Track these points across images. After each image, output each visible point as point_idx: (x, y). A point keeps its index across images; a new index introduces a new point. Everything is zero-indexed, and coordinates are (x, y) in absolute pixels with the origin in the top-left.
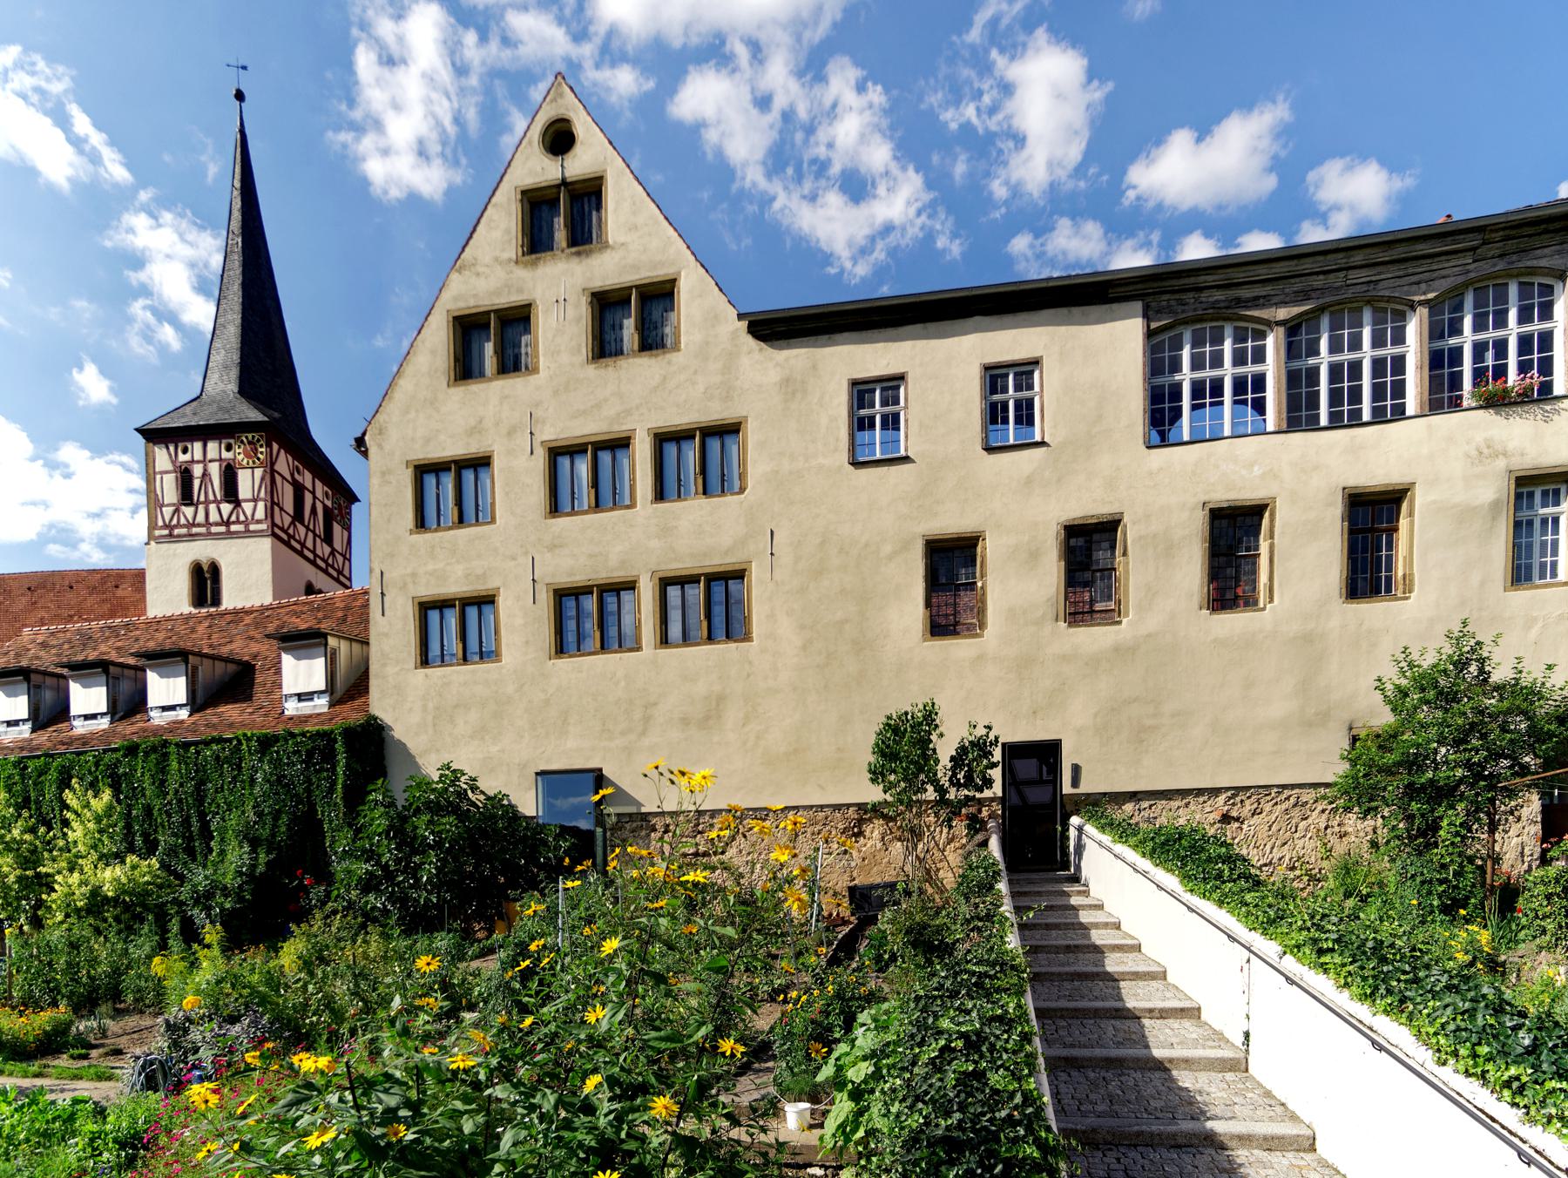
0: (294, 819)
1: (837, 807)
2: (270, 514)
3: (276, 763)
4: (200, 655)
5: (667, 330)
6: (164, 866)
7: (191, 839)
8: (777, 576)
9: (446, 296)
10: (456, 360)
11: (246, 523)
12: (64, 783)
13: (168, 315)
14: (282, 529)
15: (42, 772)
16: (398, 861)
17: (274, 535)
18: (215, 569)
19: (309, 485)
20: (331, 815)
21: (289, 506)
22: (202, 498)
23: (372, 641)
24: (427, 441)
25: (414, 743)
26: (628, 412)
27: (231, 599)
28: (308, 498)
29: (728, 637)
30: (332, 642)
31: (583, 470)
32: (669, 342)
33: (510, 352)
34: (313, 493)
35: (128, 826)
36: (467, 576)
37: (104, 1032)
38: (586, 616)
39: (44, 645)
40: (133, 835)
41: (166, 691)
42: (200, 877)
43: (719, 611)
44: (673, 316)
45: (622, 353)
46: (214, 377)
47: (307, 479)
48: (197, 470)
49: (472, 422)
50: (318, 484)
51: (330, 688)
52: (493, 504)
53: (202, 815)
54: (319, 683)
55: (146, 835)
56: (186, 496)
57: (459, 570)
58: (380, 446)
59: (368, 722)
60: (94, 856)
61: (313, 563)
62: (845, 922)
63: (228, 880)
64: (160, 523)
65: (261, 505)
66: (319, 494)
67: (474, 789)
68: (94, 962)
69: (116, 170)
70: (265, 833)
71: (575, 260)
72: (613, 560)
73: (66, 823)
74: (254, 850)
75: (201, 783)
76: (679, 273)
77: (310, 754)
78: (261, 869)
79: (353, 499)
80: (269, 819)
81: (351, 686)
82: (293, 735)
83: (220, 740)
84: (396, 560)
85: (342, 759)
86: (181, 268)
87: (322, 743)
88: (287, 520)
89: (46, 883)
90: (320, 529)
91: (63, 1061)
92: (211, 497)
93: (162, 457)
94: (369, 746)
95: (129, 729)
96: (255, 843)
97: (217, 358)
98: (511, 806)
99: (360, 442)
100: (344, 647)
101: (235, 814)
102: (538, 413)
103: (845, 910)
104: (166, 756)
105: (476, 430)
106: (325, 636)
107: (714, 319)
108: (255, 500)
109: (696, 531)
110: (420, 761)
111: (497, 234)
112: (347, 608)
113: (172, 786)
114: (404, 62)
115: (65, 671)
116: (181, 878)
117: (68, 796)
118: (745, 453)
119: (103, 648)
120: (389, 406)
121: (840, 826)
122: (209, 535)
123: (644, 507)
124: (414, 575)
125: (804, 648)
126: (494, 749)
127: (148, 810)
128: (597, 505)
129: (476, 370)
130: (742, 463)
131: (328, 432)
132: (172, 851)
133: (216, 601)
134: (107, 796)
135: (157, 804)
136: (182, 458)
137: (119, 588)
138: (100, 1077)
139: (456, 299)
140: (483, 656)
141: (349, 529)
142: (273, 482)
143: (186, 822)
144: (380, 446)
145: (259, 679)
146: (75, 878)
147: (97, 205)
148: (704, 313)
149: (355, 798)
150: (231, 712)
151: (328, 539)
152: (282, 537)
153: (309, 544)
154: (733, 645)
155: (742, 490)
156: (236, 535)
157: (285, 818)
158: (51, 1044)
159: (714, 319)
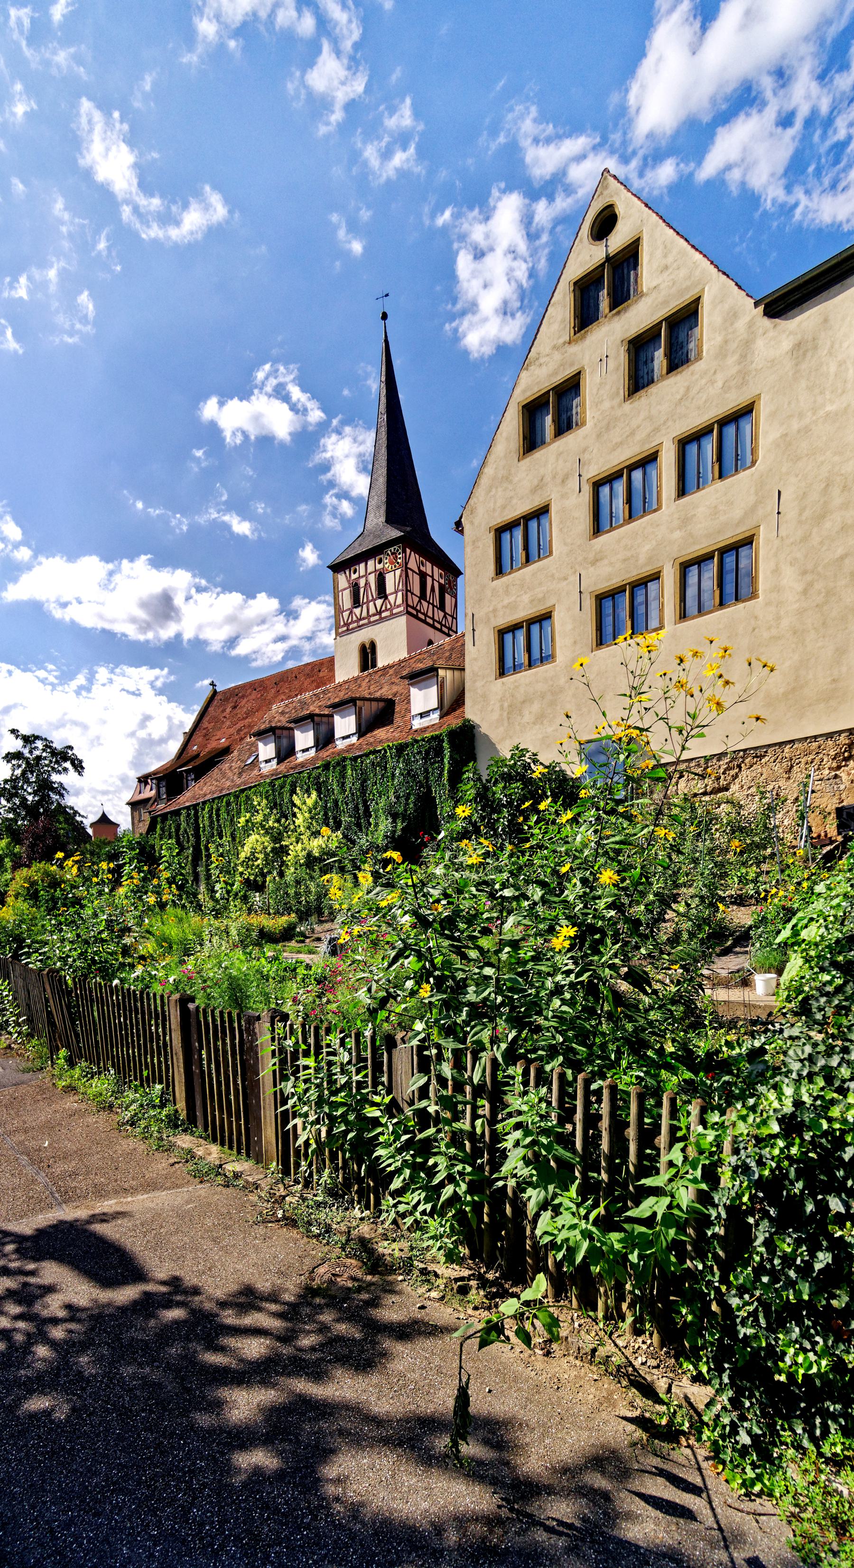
0: (419, 798)
1: (829, 736)
2: (405, 599)
3: (407, 762)
4: (364, 699)
5: (692, 345)
6: (345, 836)
7: (359, 818)
8: (782, 532)
9: (518, 391)
10: (524, 438)
11: (391, 610)
12: (293, 792)
13: (344, 495)
15: (282, 787)
16: (482, 818)
17: (408, 613)
18: (373, 645)
20: (441, 792)
21: (417, 590)
23: (467, 667)
24: (504, 507)
25: (494, 736)
26: (657, 430)
28: (429, 580)
29: (737, 599)
30: (441, 672)
31: (619, 493)
32: (692, 356)
33: (564, 417)
35: (326, 814)
36: (532, 601)
37: (313, 931)
38: (619, 610)
39: (283, 713)
40: (329, 816)
41: (345, 725)
42: (363, 841)
43: (730, 578)
44: (697, 331)
45: (653, 381)
46: (371, 516)
47: (428, 568)
48: (362, 582)
49: (536, 482)
51: (441, 706)
52: (551, 541)
53: (365, 802)
54: (434, 704)
55: (335, 818)
56: (356, 601)
57: (526, 598)
58: (472, 523)
59: (464, 725)
60: (308, 833)
61: (433, 626)
62: (831, 842)
63: (379, 842)
66: (436, 577)
67: (535, 761)
68: (308, 892)
69: (316, 415)
70: (401, 809)
71: (616, 319)
72: (642, 559)
73: (294, 815)
74: (394, 821)
75: (365, 781)
77: (427, 753)
78: (399, 833)
79: (457, 573)
80: (403, 800)
81: (453, 703)
82: (417, 741)
83: (375, 752)
84: (487, 600)
85: (447, 753)
86: (351, 461)
87: (434, 744)
88: (416, 600)
89: (284, 850)
90: (437, 602)
91: (293, 944)
93: (342, 580)
94: (465, 741)
95: (325, 754)
96: (395, 816)
97: (373, 503)
98: (562, 771)
99: (459, 524)
100: (449, 674)
101: (384, 798)
102: (586, 457)
103: (831, 829)
104: (344, 767)
105: (537, 488)
106: (436, 670)
107: (733, 316)
108: (396, 592)
109: (713, 512)
110: (498, 747)
111: (555, 327)
112: (452, 649)
113: (348, 785)
114: (492, 249)
115: (292, 725)
116: (353, 842)
117: (295, 798)
118: (757, 428)
119: (312, 708)
120: (483, 486)
121: (832, 753)
123: (668, 507)
124: (495, 610)
125: (805, 592)
126: (550, 730)
127: (336, 802)
128: (630, 517)
129: (539, 440)
130: (754, 438)
131: (439, 532)
132: (348, 828)
133: (374, 665)
134: (314, 795)
135: (341, 797)
137: (321, 670)
138: (310, 952)
139: (524, 391)
140: (543, 660)
141: (455, 597)
142: (407, 576)
143: (356, 808)
144: (472, 523)
145: (397, 709)
146: (299, 847)
147: (307, 439)
148: (728, 313)
149: (455, 778)
150: (381, 733)
151: (442, 607)
152: (412, 613)
153: (430, 614)
154: (740, 606)
155: (753, 463)
156: (387, 619)
157: (412, 798)
158: (288, 934)
159: (733, 316)
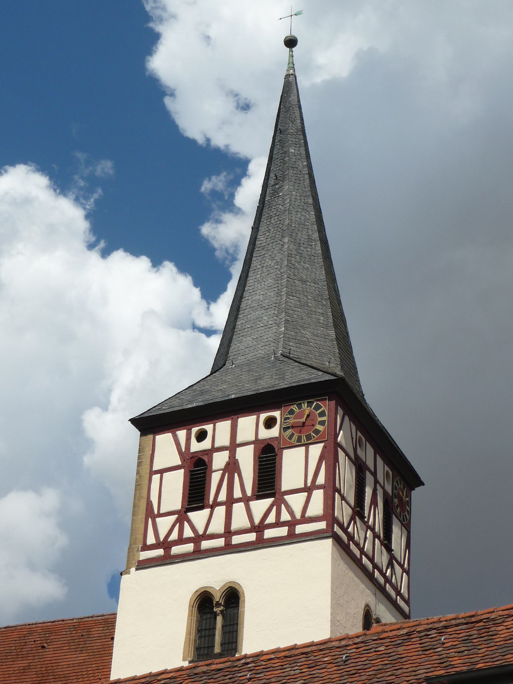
2: (329, 504)
14: (341, 526)
18: (233, 596)
19: (370, 464)
22: (223, 497)
27: (257, 636)
34: (374, 474)
48: (220, 460)
50: (380, 462)
56: (196, 495)
64: (151, 540)
65: (318, 495)
66: (380, 477)
76: (252, 159)
92: (237, 493)
108: (308, 489)
122: (230, 548)
136: (196, 447)
